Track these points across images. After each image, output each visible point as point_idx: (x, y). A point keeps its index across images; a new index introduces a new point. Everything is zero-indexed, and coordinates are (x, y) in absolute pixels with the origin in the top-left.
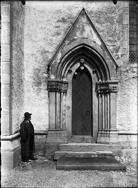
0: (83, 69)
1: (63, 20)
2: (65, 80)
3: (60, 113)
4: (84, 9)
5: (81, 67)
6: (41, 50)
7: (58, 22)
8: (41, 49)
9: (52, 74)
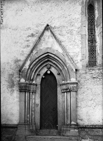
0: (49, 73)
1: (33, 35)
2: (34, 82)
3: (67, 105)
4: (48, 25)
5: (48, 72)
6: (15, 59)
7: (28, 37)
8: (15, 59)
9: (22, 77)
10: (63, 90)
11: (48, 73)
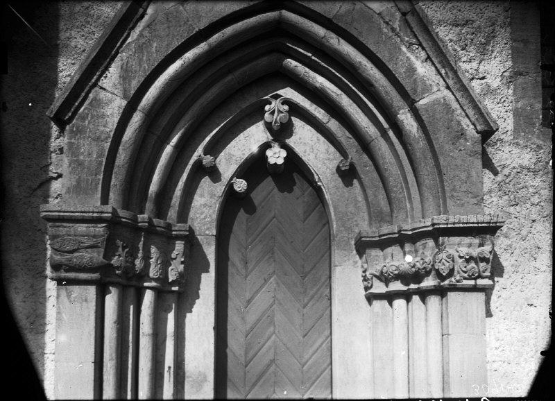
0: (280, 161)
5: (269, 153)
10: (385, 278)
11: (272, 161)
